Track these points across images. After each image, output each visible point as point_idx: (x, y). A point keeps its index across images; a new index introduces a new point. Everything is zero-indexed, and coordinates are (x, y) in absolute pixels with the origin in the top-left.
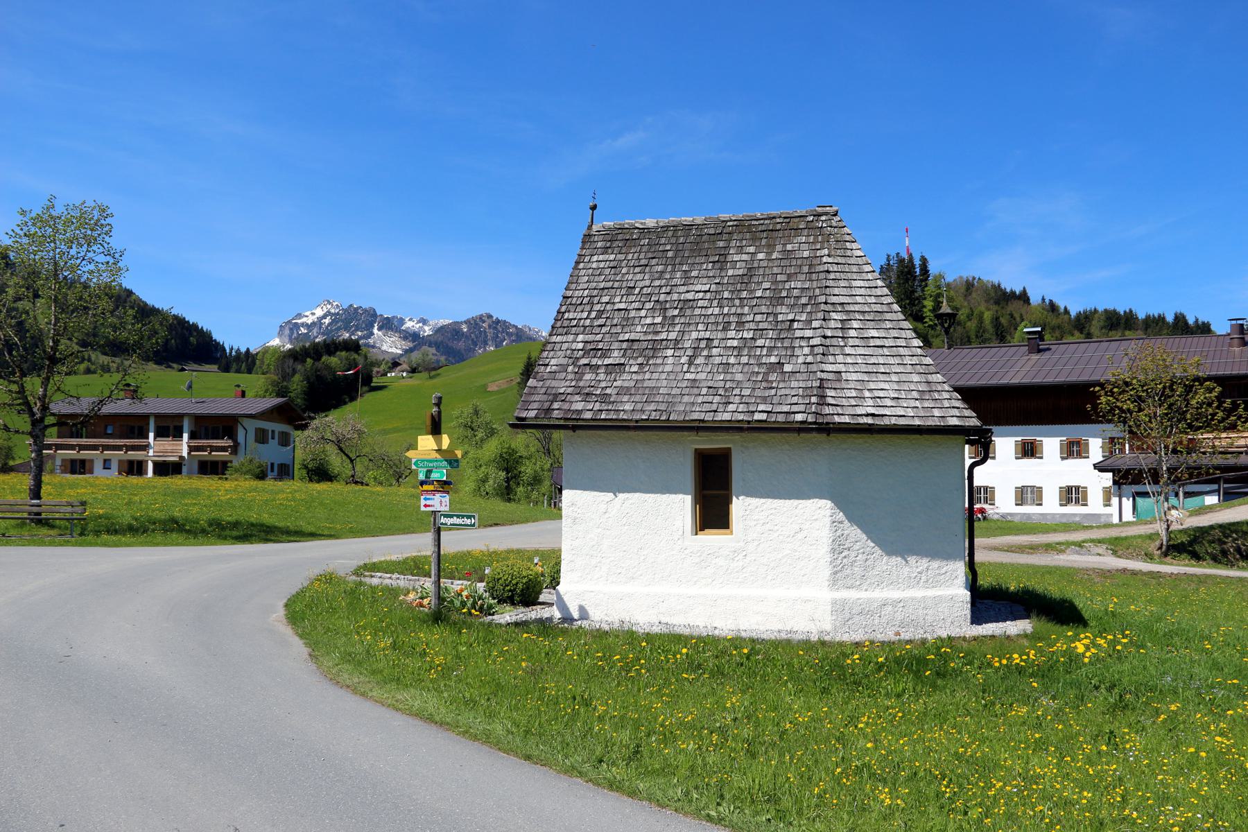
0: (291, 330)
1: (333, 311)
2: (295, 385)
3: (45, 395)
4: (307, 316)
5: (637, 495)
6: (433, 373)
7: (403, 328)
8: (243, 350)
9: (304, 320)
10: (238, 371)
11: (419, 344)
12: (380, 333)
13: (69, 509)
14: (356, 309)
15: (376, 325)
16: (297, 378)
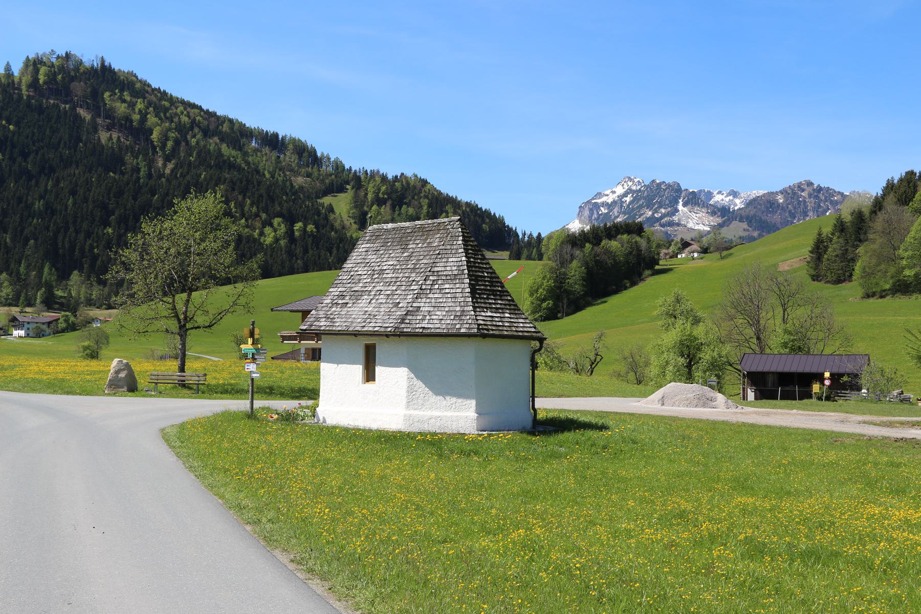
0: (591, 210)
1: (634, 188)
2: (573, 271)
3: (186, 311)
4: (607, 195)
5: (345, 365)
6: (725, 253)
7: (711, 202)
8: (535, 235)
9: (604, 199)
10: (529, 258)
11: (728, 219)
12: (685, 209)
13: (197, 378)
14: (659, 185)
15: (680, 201)
16: (575, 264)
